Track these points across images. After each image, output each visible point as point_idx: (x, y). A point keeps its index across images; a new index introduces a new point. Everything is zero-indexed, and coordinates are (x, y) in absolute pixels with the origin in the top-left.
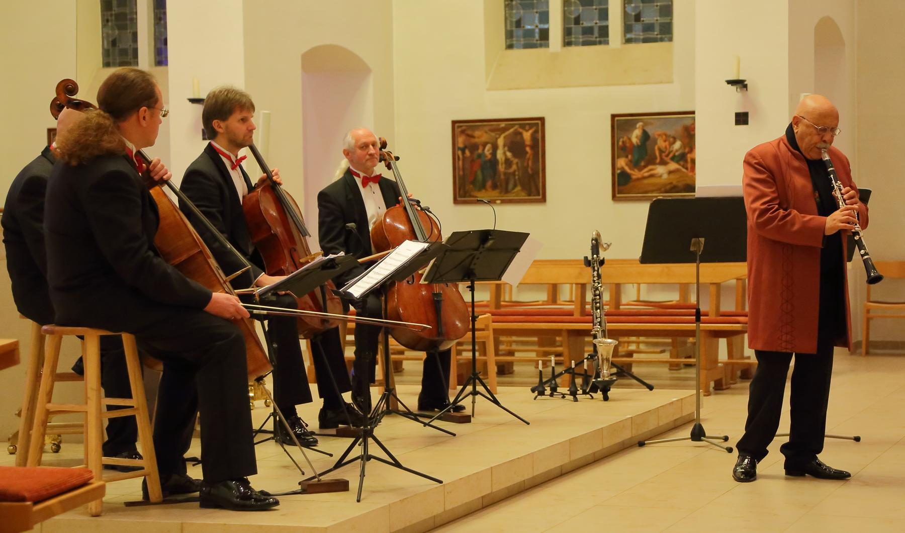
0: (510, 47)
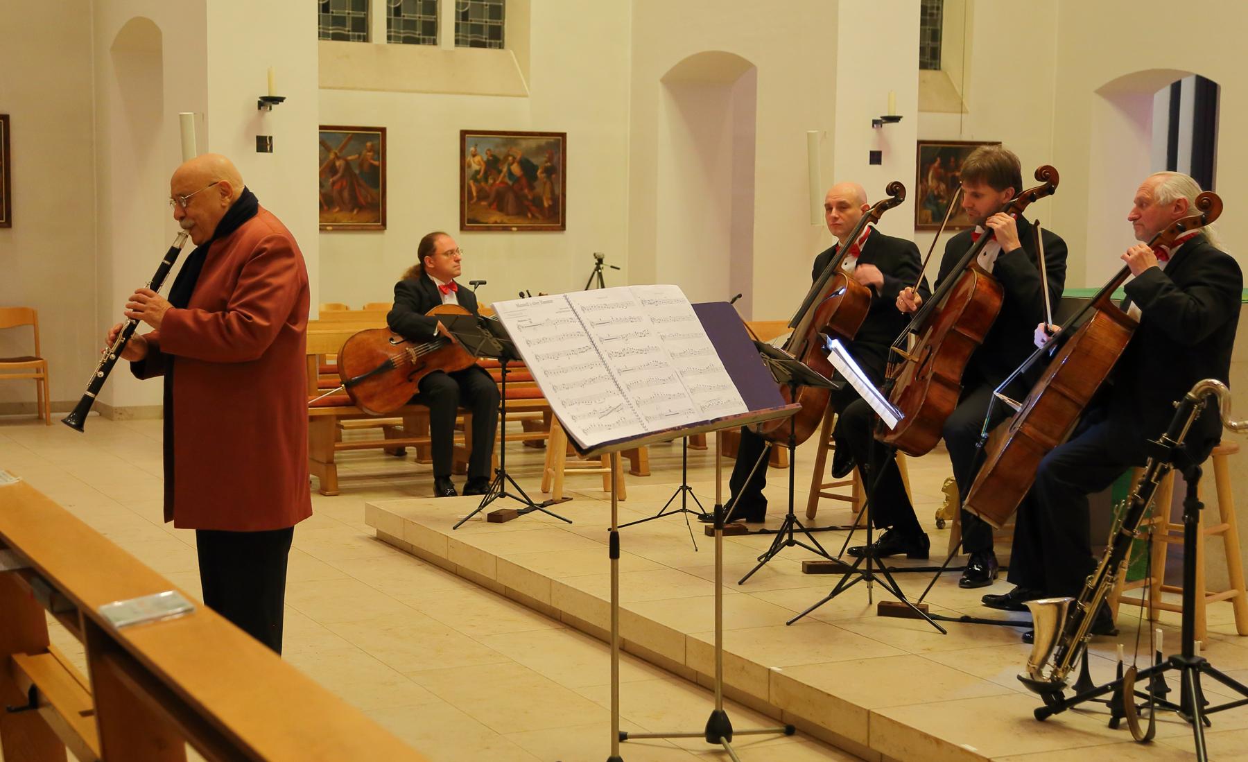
0: (321, 127)
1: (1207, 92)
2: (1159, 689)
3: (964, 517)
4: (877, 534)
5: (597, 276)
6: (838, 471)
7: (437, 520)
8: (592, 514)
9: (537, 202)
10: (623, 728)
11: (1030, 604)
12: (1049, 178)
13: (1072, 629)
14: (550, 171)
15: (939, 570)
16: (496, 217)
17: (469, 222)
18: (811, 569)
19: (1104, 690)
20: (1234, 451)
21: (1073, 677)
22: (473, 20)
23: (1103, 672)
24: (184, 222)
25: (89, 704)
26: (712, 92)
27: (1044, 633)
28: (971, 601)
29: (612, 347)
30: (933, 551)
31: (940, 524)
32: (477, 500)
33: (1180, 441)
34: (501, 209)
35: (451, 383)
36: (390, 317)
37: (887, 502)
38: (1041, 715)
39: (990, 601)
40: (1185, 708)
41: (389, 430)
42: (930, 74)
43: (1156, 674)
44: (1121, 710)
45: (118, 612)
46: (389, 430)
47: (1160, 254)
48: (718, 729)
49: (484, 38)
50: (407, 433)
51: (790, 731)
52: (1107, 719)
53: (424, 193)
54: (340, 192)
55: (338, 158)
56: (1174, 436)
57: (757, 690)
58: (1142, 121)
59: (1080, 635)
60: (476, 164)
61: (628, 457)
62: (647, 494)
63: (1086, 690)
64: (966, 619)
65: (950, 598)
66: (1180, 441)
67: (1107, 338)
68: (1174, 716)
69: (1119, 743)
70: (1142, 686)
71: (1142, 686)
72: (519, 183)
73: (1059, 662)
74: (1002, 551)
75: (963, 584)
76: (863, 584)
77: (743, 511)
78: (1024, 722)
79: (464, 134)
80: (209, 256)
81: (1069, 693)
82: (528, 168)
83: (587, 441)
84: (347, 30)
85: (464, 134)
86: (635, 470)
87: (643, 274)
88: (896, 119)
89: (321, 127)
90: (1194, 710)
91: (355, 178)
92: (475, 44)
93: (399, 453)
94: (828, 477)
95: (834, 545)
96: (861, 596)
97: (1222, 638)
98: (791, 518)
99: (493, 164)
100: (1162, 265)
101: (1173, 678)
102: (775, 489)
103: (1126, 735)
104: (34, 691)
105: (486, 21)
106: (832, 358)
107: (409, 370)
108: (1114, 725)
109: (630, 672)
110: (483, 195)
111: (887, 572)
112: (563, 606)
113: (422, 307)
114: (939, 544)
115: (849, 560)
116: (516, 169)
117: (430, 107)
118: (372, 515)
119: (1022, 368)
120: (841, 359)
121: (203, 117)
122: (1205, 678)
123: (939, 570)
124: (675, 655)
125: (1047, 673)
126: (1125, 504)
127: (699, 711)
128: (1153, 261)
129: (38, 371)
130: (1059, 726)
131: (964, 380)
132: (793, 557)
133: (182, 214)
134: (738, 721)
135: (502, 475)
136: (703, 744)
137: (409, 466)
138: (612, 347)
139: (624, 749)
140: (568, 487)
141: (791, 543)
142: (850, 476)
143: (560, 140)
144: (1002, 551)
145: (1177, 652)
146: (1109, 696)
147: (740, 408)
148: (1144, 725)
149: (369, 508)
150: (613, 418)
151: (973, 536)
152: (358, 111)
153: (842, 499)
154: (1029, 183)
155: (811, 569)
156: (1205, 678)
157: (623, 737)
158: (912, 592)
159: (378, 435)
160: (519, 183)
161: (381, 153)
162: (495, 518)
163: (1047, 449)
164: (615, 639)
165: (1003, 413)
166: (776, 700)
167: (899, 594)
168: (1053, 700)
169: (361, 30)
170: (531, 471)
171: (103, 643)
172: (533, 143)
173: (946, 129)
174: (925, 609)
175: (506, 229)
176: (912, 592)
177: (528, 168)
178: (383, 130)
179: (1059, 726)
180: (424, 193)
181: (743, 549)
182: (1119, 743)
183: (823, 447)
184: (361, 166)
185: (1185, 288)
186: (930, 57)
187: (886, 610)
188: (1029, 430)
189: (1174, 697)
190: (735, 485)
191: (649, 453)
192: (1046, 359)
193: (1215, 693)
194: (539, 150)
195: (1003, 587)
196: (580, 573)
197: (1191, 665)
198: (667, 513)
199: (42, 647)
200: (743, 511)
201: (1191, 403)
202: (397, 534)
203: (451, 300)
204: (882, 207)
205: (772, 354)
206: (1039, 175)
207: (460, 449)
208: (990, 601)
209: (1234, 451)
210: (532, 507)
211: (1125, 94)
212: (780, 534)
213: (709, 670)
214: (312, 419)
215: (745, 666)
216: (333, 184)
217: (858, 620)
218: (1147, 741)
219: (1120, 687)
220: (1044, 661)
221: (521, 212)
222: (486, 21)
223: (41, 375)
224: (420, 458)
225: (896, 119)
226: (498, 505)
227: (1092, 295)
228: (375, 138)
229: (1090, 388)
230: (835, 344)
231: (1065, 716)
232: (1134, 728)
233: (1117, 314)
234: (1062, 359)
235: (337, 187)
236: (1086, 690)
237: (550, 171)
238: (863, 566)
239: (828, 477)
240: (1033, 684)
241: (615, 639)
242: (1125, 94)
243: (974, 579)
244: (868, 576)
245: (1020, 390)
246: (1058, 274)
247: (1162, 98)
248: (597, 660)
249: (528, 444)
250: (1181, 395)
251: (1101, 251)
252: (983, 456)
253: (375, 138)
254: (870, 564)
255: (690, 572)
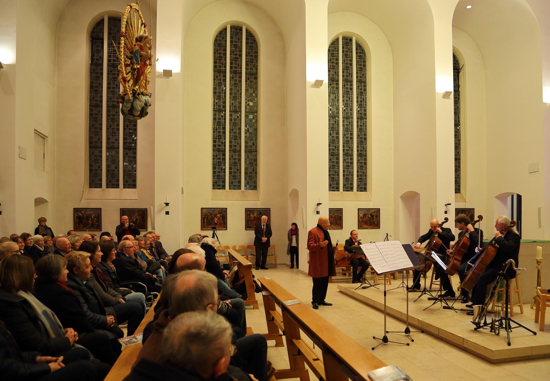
1: (519, 197)
2: (501, 324)
3: (462, 289)
4: (443, 293)
5: (387, 238)
6: (436, 279)
7: (352, 288)
8: (381, 287)
9: (374, 223)
10: (387, 330)
11: (473, 306)
12: (481, 217)
13: (482, 311)
14: (377, 216)
15: (456, 300)
16: (365, 226)
17: (360, 227)
18: (429, 299)
19: (489, 324)
20: (519, 274)
21: (483, 322)
22: (360, 186)
23: (489, 321)
25: (282, 320)
26: (411, 200)
27: (476, 312)
28: (463, 306)
29: (385, 253)
30: (456, 295)
31: (458, 290)
32: (359, 284)
33: (505, 272)
34: (366, 224)
35: (357, 261)
36: (345, 247)
37: (446, 284)
38: (476, 329)
39: (467, 306)
40: (506, 328)
41: (343, 270)
42: (458, 194)
43: (501, 320)
44: (493, 328)
45: (288, 303)
46: (343, 270)
47: (501, 233)
48: (407, 331)
49: (363, 190)
50: (346, 270)
51: (423, 332)
52: (490, 330)
53: (350, 221)
56: (503, 271)
57: (416, 324)
58: (505, 203)
59: (484, 313)
60: (361, 215)
61: (393, 275)
62: (396, 283)
63: (485, 324)
64: (462, 310)
65: (459, 305)
66: (505, 272)
67: (492, 251)
68: (504, 330)
69: (492, 335)
70: (497, 323)
71: (497, 323)
72: (370, 219)
73: (479, 318)
74: (470, 295)
75: (462, 303)
76: (440, 302)
77: (416, 287)
78: (472, 331)
79: (359, 209)
81: (482, 325)
82: (372, 216)
83: (379, 272)
84: (335, 189)
85: (359, 209)
86: (394, 278)
87: (396, 239)
88: (450, 204)
90: (508, 328)
91: (336, 217)
92: (361, 191)
93: (345, 274)
94: (434, 280)
95: (434, 294)
96: (439, 305)
97: (517, 314)
98: (425, 288)
99: (365, 215)
100: (503, 236)
101: (504, 321)
102: (422, 282)
103: (494, 333)
104: (273, 317)
105: (363, 186)
106: (432, 255)
107: (349, 258)
108: (491, 331)
109: (388, 318)
110: (362, 222)
111: (445, 300)
112: (535, 353)
113: (351, 245)
114: (457, 294)
115: (437, 297)
116: (369, 216)
117: (351, 204)
118: (339, 287)
119: (474, 258)
120: (435, 256)
121: (306, 208)
122: (511, 322)
123: (456, 300)
124: (400, 316)
125: (477, 321)
126: (493, 285)
127: (403, 327)
128: (500, 235)
130: (479, 332)
131: (462, 259)
132: (426, 297)
134: (411, 329)
135: (365, 279)
136: (404, 334)
137: (347, 277)
138: (385, 253)
139: (387, 334)
140: (379, 282)
141: (425, 294)
142: (439, 280)
143: (378, 210)
144: (470, 295)
145: (504, 316)
146: (490, 325)
147: (412, 266)
148: (497, 332)
150: (385, 268)
151: (464, 292)
152: (337, 205)
153: (437, 285)
154: (476, 219)
155: (429, 299)
156: (511, 322)
157: (387, 332)
158: (450, 304)
159: (341, 271)
160: (370, 219)
161: (342, 213)
162: (364, 288)
163: (479, 274)
164: (386, 312)
165: (470, 267)
166: (420, 325)
167: (447, 304)
168: (478, 326)
169: (338, 189)
170: (372, 278)
171: (285, 309)
172: (373, 211)
173: (462, 206)
174: (453, 308)
175: (368, 228)
176: (450, 304)
177: (372, 216)
179: (479, 332)
180: (350, 221)
181: (413, 295)
182: (492, 335)
183: (433, 274)
185: (507, 241)
186: (458, 190)
187: (444, 308)
188: (476, 271)
189: (504, 326)
190: (414, 282)
191: (397, 274)
192: (479, 255)
193: (513, 325)
194: (374, 212)
195: (470, 303)
196: (379, 299)
197: (508, 319)
198: (397, 286)
199: (274, 310)
200: (416, 287)
201: (506, 264)
202: (344, 291)
203: (356, 244)
204: (443, 223)
205: (421, 254)
206: (478, 217)
208: (467, 306)
209: (519, 274)
210: (371, 286)
211: (501, 198)
212: (423, 292)
213: (405, 319)
215: (413, 318)
217: (439, 310)
218: (498, 334)
219: (493, 323)
220: (476, 318)
221: (371, 225)
222: (363, 186)
224: (349, 275)
225: (450, 204)
226: (364, 285)
227: (489, 241)
228: (340, 211)
229: (489, 262)
230: (433, 252)
231: (481, 329)
232: (495, 332)
233: (493, 246)
234: (483, 256)
236: (485, 324)
237: (377, 216)
238: (440, 298)
239: (434, 280)
240: (474, 323)
241: (386, 312)
242: (501, 198)
243: (464, 301)
244: (441, 301)
245: (473, 262)
246: (482, 236)
247: (510, 198)
248: (382, 316)
249: (372, 273)
250: (505, 263)
251: (490, 232)
252: (466, 276)
253: (340, 211)
254: (441, 298)
255: (403, 299)
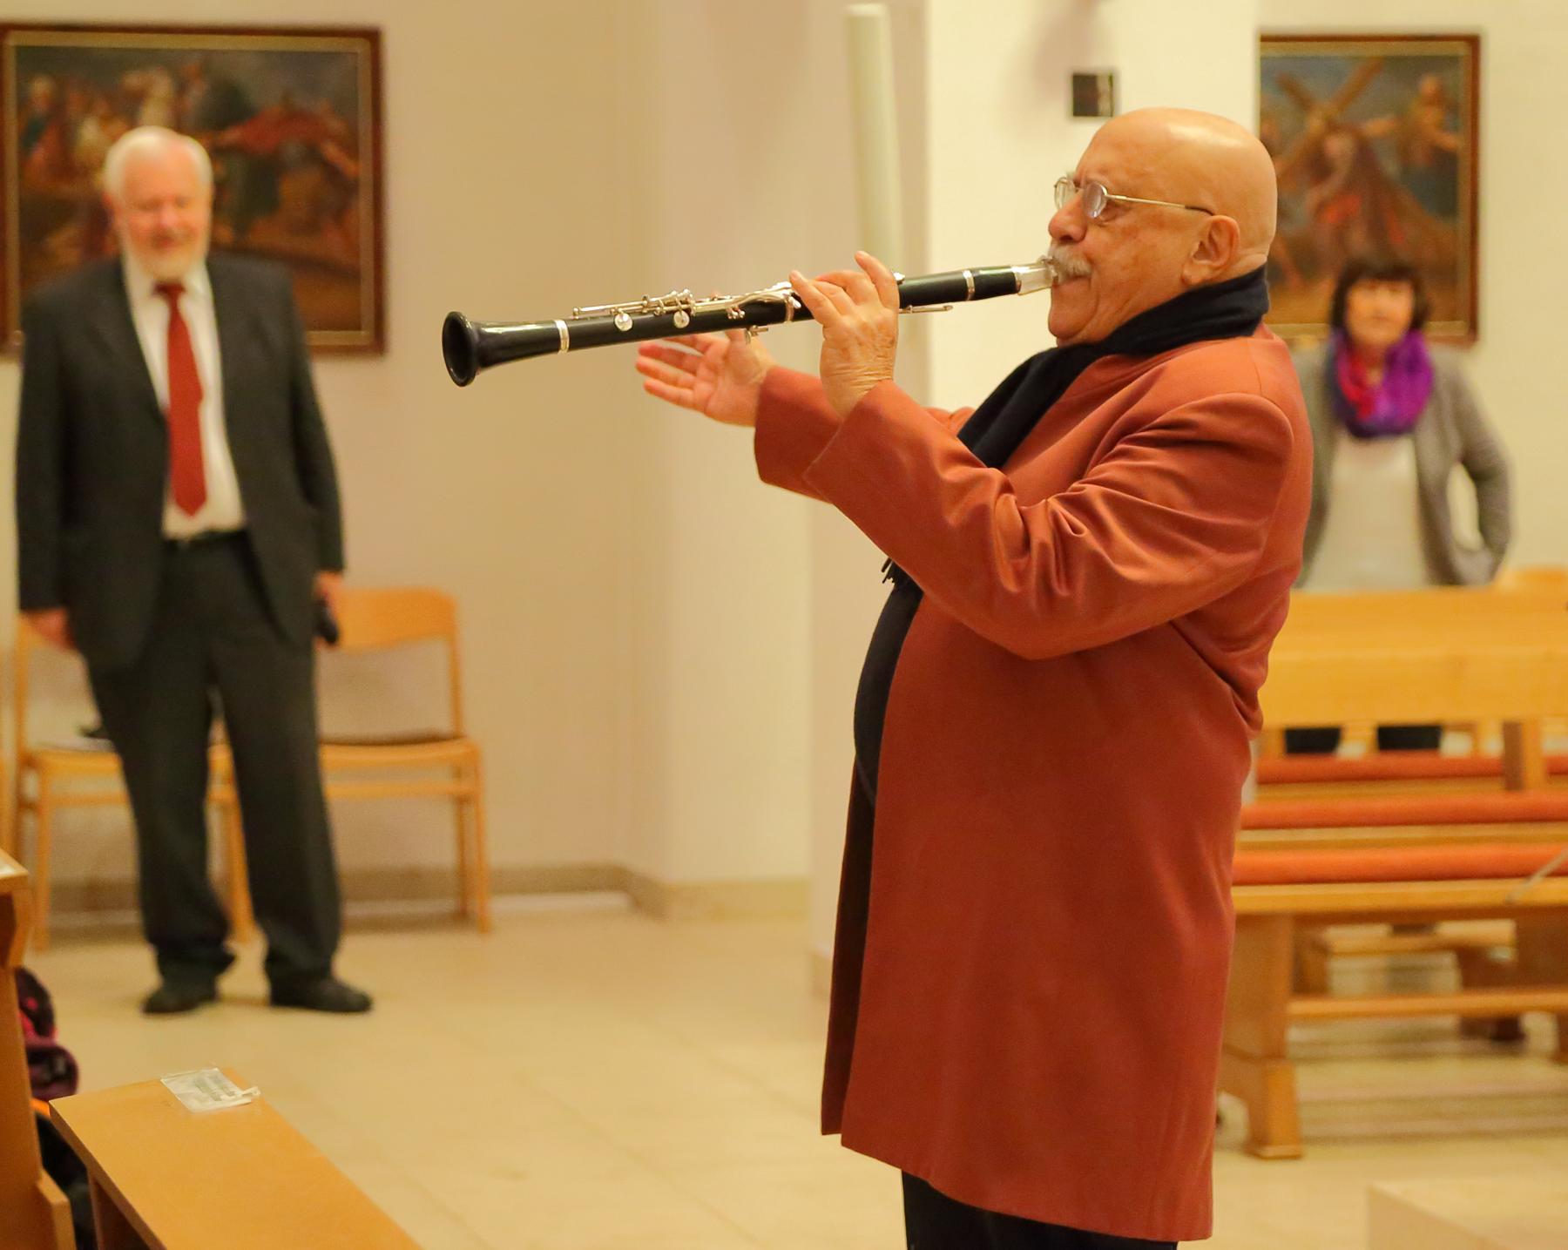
0: (1266, 39)
24: (1064, 252)
50: (1524, 974)
54: (1340, 235)
55: (1332, 127)
80: (1073, 393)
89: (1266, 39)
93: (1504, 1034)
129: (458, 773)
133: (1073, 230)
149: (1383, 1209)
161: (1464, 109)
178: (1473, 42)
184: (1404, 152)
207: (61, 1206)
214: (1249, 921)
216: (1321, 208)
223: (464, 787)
228: (1446, 69)
235: (1331, 218)
253: (1446, 69)
